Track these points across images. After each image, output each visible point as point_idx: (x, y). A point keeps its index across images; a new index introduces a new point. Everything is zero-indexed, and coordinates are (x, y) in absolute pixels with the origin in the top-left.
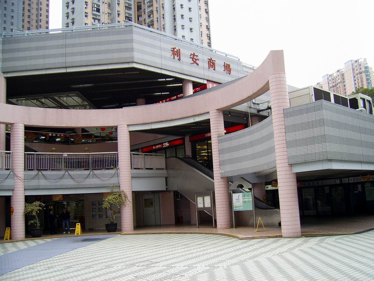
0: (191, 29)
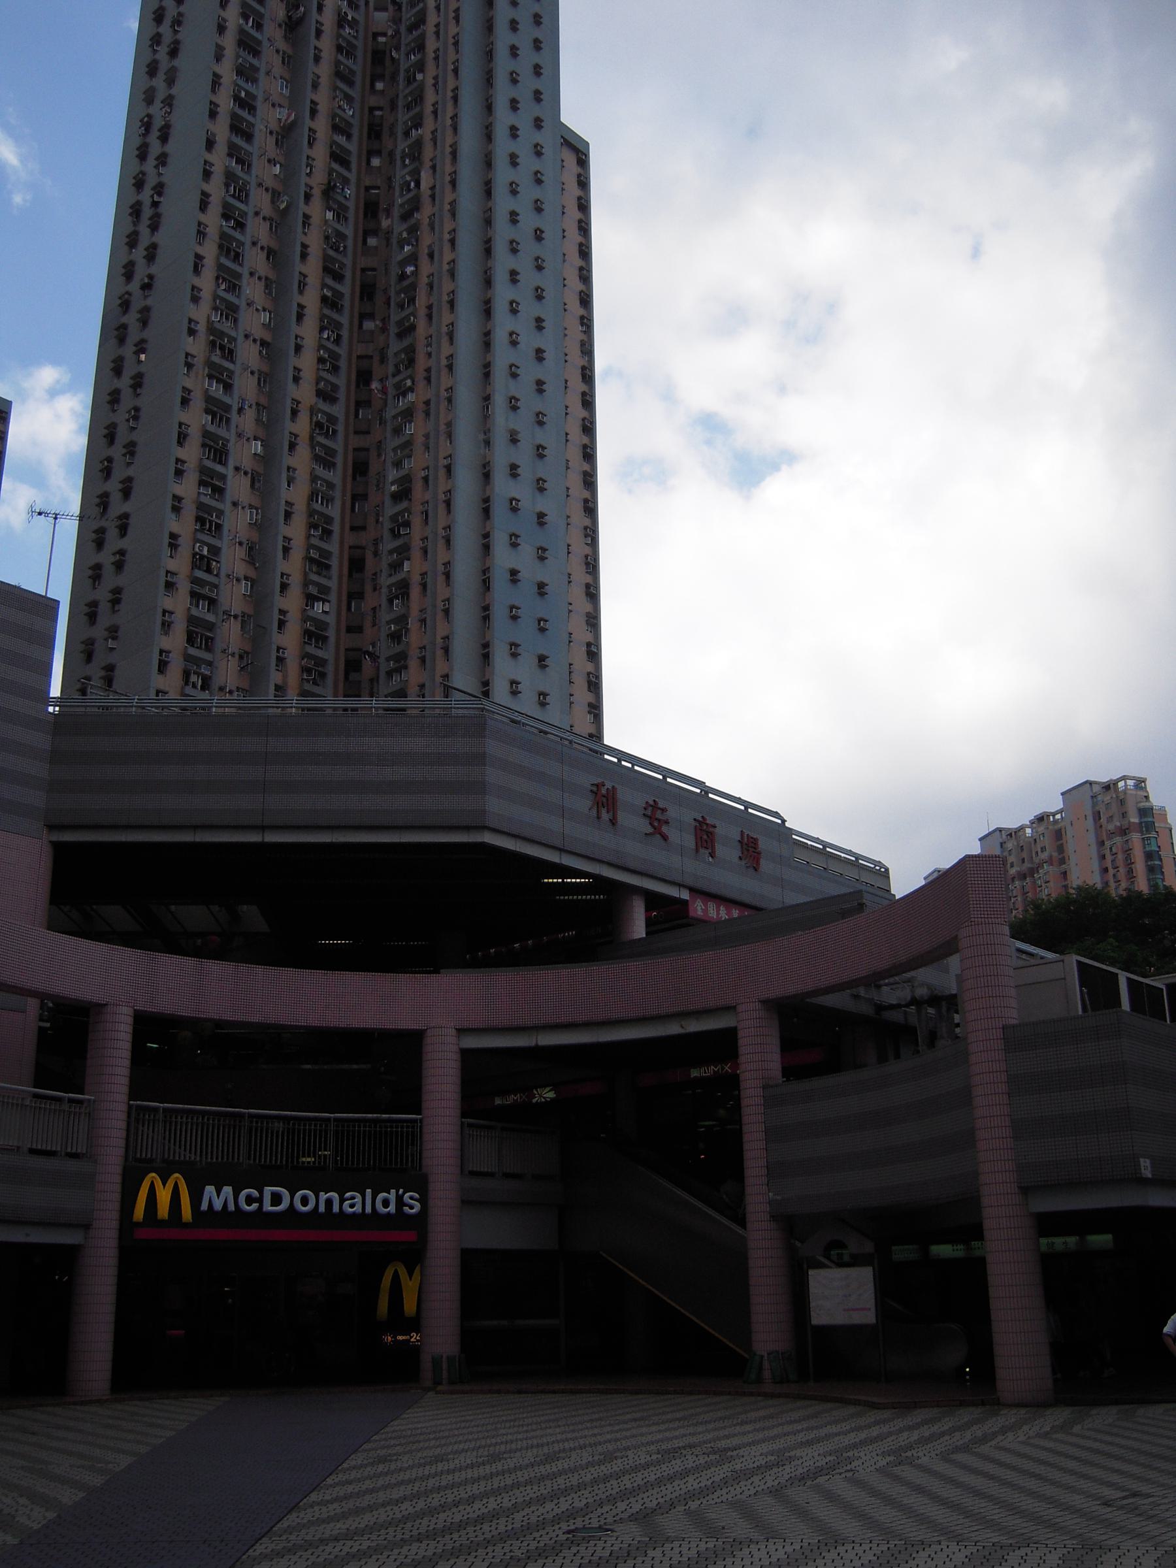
0: (542, 659)
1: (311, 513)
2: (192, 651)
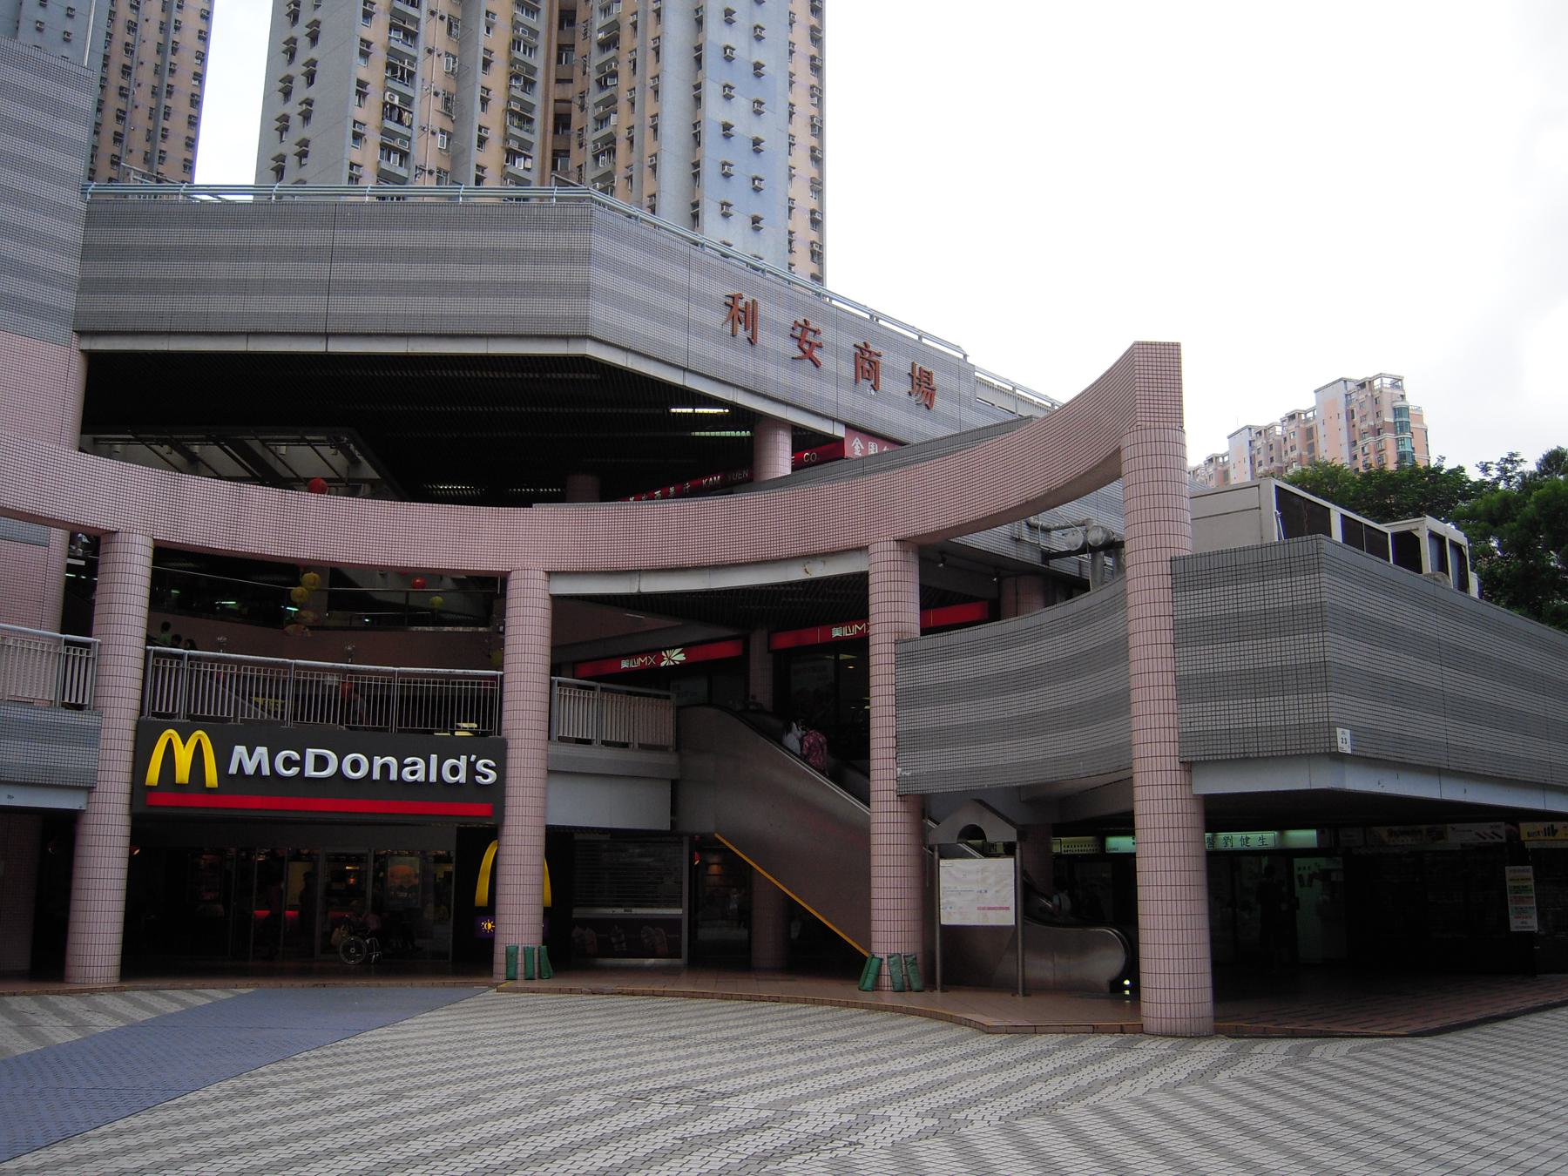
0: (756, 220)
1: (513, 62)
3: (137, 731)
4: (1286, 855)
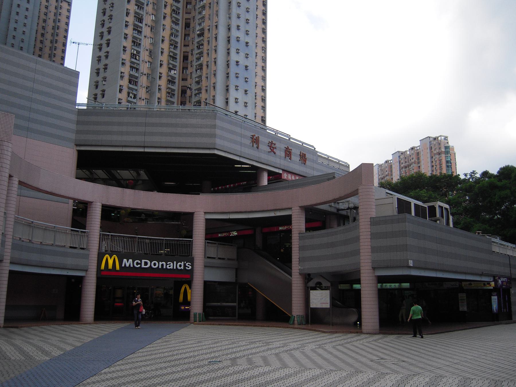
0: (246, 91)
2: (131, 86)
3: (98, 255)
4: (401, 290)
